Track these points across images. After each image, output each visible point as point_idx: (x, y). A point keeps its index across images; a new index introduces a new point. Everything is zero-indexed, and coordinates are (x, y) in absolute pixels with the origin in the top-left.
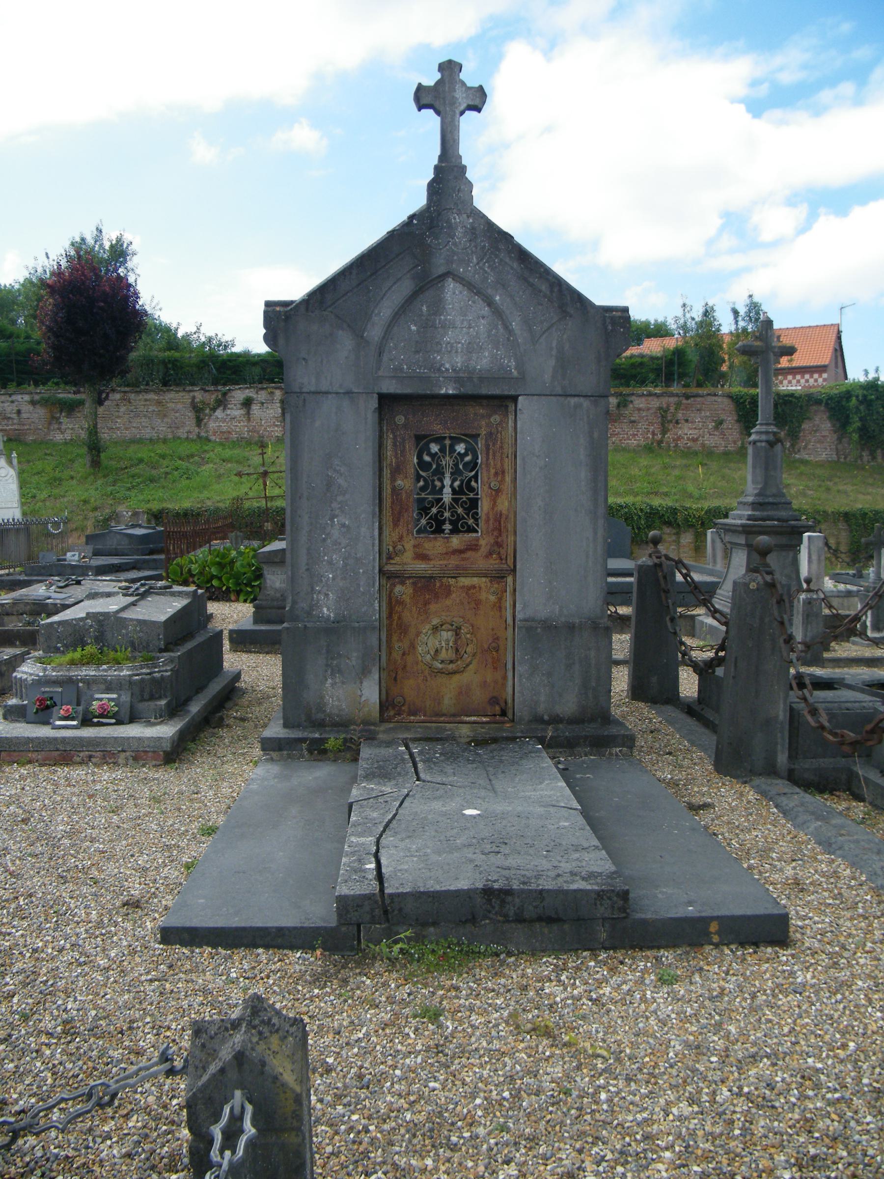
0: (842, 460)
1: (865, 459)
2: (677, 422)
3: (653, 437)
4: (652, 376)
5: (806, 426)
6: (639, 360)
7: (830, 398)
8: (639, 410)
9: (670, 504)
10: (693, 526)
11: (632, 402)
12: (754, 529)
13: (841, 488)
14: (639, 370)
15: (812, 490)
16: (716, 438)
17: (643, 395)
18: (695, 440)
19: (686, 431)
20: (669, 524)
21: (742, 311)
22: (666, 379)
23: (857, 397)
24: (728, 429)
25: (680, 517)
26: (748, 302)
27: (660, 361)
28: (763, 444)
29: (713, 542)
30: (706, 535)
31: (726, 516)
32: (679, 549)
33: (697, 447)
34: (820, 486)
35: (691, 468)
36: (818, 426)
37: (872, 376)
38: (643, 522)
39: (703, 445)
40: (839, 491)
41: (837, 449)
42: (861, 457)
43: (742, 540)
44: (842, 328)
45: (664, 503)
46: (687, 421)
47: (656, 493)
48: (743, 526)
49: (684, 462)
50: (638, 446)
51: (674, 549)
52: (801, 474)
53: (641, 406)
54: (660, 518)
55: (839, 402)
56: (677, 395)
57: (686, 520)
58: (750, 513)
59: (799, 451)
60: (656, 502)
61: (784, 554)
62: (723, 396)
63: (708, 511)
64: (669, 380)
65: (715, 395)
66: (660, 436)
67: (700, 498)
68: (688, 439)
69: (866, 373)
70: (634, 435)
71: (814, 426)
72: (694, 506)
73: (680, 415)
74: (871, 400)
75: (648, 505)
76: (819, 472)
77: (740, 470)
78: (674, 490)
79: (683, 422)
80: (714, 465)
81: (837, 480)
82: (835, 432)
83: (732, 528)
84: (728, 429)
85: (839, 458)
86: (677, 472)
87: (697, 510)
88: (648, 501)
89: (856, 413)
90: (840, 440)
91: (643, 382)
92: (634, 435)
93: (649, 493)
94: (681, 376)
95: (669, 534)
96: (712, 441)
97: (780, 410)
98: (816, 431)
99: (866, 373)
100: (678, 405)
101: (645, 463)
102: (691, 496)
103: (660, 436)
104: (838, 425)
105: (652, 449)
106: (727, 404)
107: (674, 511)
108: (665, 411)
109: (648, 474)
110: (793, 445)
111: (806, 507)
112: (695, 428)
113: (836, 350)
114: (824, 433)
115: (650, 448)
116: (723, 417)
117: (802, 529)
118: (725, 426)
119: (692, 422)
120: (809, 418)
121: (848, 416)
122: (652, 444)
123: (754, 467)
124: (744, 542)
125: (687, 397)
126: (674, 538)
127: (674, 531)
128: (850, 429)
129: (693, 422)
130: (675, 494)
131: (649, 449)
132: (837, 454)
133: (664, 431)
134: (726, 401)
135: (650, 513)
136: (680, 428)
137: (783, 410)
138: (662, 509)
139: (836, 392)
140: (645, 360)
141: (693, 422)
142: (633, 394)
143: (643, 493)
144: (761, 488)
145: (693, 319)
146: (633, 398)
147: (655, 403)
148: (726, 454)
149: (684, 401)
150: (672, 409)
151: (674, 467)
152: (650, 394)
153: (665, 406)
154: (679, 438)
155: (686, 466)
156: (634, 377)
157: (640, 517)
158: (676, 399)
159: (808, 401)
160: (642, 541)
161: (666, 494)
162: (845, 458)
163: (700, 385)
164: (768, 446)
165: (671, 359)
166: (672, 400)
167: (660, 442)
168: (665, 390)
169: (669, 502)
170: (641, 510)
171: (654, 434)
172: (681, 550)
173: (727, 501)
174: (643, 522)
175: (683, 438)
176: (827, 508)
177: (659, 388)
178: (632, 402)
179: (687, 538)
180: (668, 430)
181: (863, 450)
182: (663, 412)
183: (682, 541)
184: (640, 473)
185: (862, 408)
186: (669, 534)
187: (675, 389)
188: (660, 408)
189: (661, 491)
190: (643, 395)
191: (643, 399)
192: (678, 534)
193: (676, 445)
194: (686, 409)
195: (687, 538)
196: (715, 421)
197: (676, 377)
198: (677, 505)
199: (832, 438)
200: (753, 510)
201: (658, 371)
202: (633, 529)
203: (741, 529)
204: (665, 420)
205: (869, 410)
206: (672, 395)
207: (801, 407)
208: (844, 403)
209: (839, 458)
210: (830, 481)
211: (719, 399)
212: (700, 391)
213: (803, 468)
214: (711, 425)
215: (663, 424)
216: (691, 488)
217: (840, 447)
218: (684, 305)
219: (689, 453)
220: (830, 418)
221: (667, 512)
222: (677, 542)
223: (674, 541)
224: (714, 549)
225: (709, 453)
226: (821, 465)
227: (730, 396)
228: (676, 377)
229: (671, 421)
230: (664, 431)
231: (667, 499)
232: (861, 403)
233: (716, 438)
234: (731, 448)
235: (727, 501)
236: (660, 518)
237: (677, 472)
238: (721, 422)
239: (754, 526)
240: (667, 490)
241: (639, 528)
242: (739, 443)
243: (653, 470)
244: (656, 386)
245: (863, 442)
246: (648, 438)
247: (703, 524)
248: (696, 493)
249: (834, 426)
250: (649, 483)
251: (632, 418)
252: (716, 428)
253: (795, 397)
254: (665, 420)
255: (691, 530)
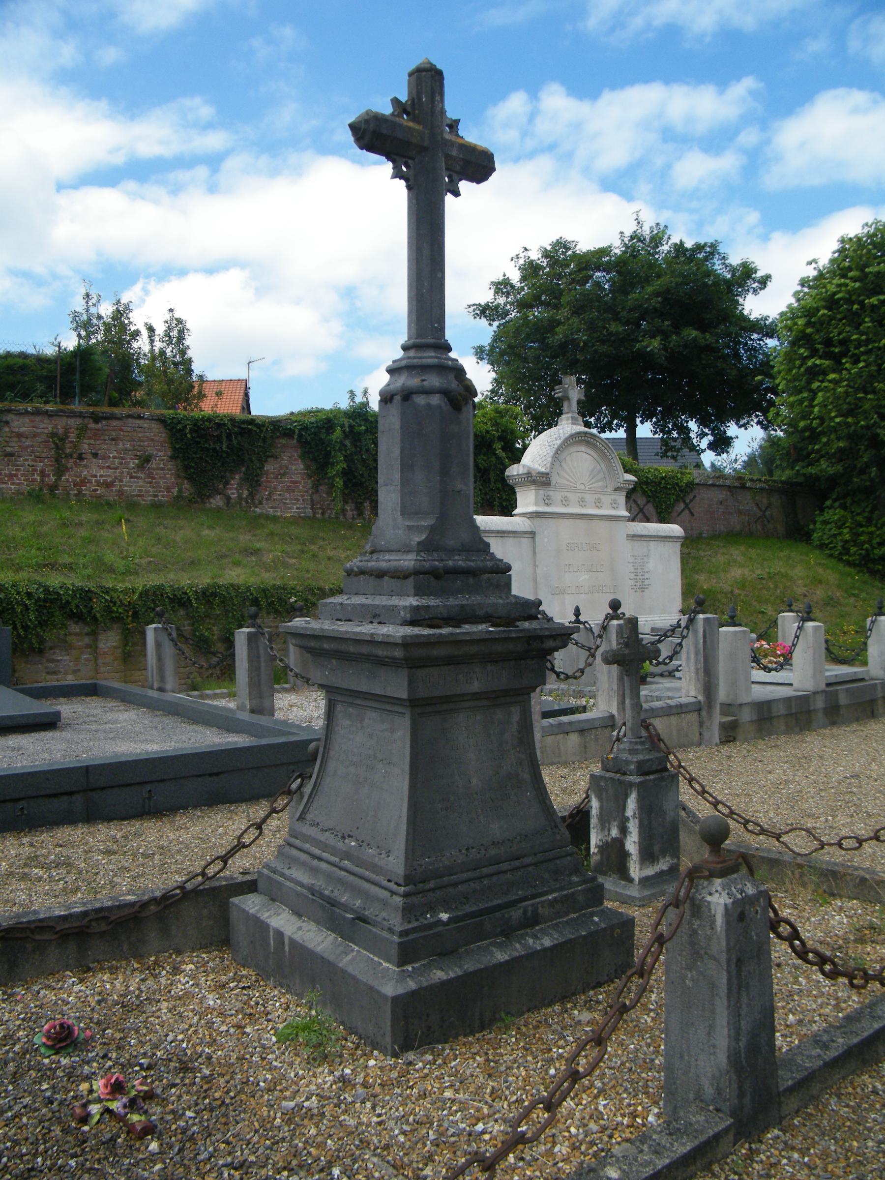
0: (319, 516)
1: (349, 514)
2: (81, 458)
3: (42, 480)
4: (40, 387)
5: (270, 467)
6: (21, 361)
7: (305, 428)
8: (20, 435)
9: (79, 584)
10: (118, 619)
11: (7, 423)
12: (435, 652)
13: (330, 553)
14: (19, 377)
15: (293, 557)
16: (141, 483)
17: (27, 413)
18: (108, 485)
19: (95, 471)
20: (78, 617)
21: (160, 329)
22: (61, 394)
23: (342, 426)
24: (158, 469)
25: (97, 606)
26: (167, 317)
27: (52, 366)
28: (435, 400)
29: (158, 645)
30: (143, 634)
31: (307, 608)
32: (96, 659)
33: (112, 497)
34: (303, 551)
35: (107, 527)
36: (287, 468)
37: (359, 399)
38: (32, 617)
39: (121, 493)
40: (329, 559)
41: (312, 500)
42: (344, 511)
43: (396, 686)
44: (251, 384)
45: (69, 583)
46: (95, 455)
47: (53, 566)
48: (407, 644)
49: (95, 517)
50: (19, 493)
51: (87, 660)
52: (272, 534)
53: (23, 429)
54: (62, 607)
55: (315, 434)
56: (81, 415)
57: (108, 609)
58: (413, 601)
59: (260, 503)
60: (54, 580)
61: (499, 714)
62: (152, 419)
63: (145, 593)
64: (67, 395)
65: (139, 417)
66: (53, 478)
67: (128, 572)
68: (98, 483)
69: (352, 394)
70: (11, 476)
71: (281, 467)
72: (120, 586)
73: (85, 447)
74: (359, 433)
75: (40, 584)
76: (294, 530)
77: (181, 528)
78: (82, 561)
79: (90, 456)
80: (142, 523)
81: (321, 543)
82: (310, 477)
83: (381, 652)
84: (158, 469)
85: (314, 514)
86: (83, 533)
87: (125, 592)
88: (38, 578)
89: (340, 450)
90: (316, 487)
91: (25, 396)
92: (11, 476)
93: (40, 566)
94: (86, 389)
95: (76, 634)
96: (134, 486)
97: (235, 442)
98: (284, 474)
99: (352, 394)
100: (82, 431)
101: (32, 518)
102: (112, 570)
103: (53, 478)
104: (314, 467)
105: (43, 495)
106: (157, 432)
107: (86, 595)
108: (62, 440)
109: (38, 535)
110: (252, 495)
111: (292, 583)
112: (108, 467)
113: (243, 408)
114: (295, 478)
115: (38, 497)
116: (150, 450)
117: (550, 644)
118: (153, 464)
119: (104, 458)
120: (276, 457)
121: (328, 454)
122: (41, 489)
123: (407, 466)
124: (404, 695)
125: (97, 419)
126: (87, 640)
127: (87, 629)
128: (332, 472)
129: (105, 458)
130: (85, 567)
131: (36, 497)
132: (312, 508)
133: (60, 471)
134: (156, 427)
135: (45, 600)
136: (85, 466)
137: (239, 443)
138: (66, 593)
139: (313, 420)
140: (28, 362)
141: (105, 458)
142: (9, 411)
143: (29, 566)
144: (433, 529)
145: (100, 317)
146: (10, 417)
147: (46, 426)
148: (156, 506)
149: (92, 425)
150: (73, 437)
151: (81, 524)
152: (38, 413)
153: (61, 431)
154: (84, 482)
155: (97, 523)
156: (12, 387)
157: (27, 608)
158: (79, 421)
159: (273, 431)
160: (32, 649)
161: (70, 567)
162: (323, 514)
163: (113, 403)
164: (446, 407)
165: (70, 364)
166: (74, 422)
167: (53, 488)
168: (62, 407)
169: (75, 581)
170: (29, 595)
171: (43, 474)
172: (100, 661)
173: (172, 576)
174: (32, 617)
175: (90, 482)
176: (321, 584)
177: (51, 404)
178: (7, 423)
179: (109, 640)
180: (67, 469)
181: (345, 502)
182: (58, 441)
183: (101, 645)
184: (23, 534)
185: (347, 443)
186: (76, 634)
187: (77, 406)
188: (54, 435)
189: (60, 561)
190: (27, 413)
191: (27, 420)
192: (94, 634)
193: (80, 492)
194: (96, 435)
195: (109, 640)
196: (139, 457)
197: (77, 390)
198: (91, 585)
199: (304, 485)
200: (419, 592)
201: (49, 380)
202: (15, 628)
203: (398, 653)
204: (62, 453)
205: (356, 446)
206: (73, 415)
207: (264, 439)
208: (323, 436)
209: (314, 514)
210: (314, 544)
211: (146, 424)
212: (116, 411)
213: (271, 526)
214: (133, 463)
215: (57, 460)
216: (110, 557)
217: (316, 497)
218: (88, 295)
219: (100, 504)
220: (303, 457)
221: (74, 596)
222: (93, 647)
223: (88, 646)
224: (160, 659)
225: (132, 505)
226: (295, 521)
227: (162, 420)
228: (77, 390)
229: (71, 456)
230: (60, 471)
231: (72, 575)
232: (346, 435)
233: (141, 483)
234: (162, 497)
235: (172, 576)
236: (62, 607)
237: (83, 533)
238: (148, 460)
239: (441, 641)
240: (71, 560)
241: (26, 628)
242: (175, 491)
243: (45, 529)
244: (46, 402)
245: (346, 492)
246: (34, 480)
247: (135, 615)
248: (120, 565)
249: (307, 467)
250: (39, 549)
251: (8, 449)
252: (141, 467)
253: (257, 425)
254: (62, 453)
255: (115, 626)
